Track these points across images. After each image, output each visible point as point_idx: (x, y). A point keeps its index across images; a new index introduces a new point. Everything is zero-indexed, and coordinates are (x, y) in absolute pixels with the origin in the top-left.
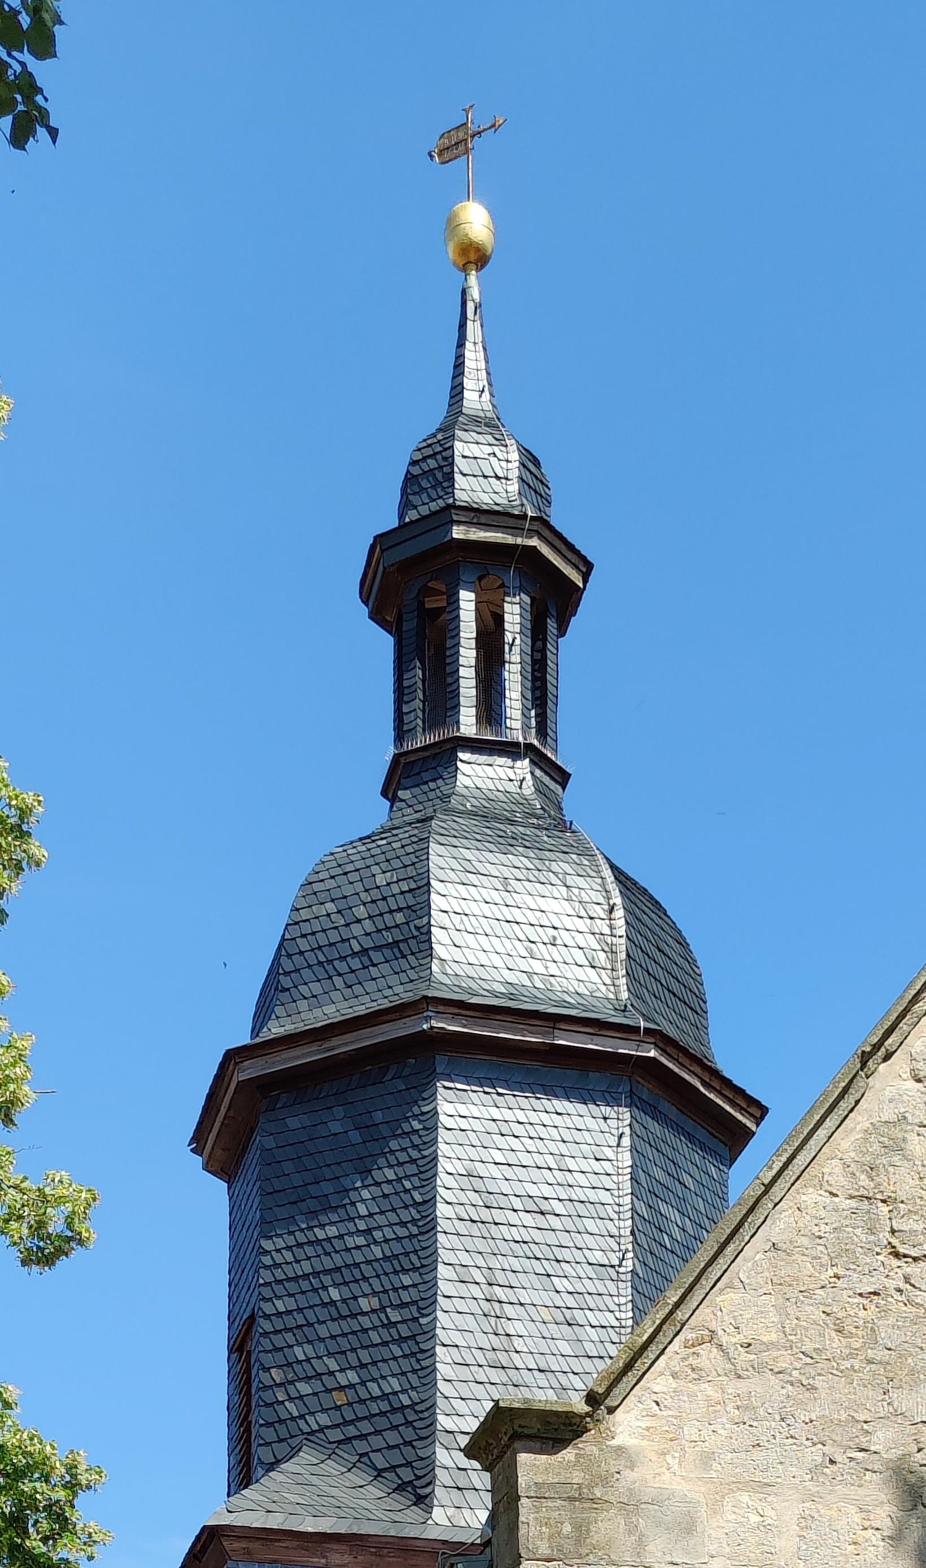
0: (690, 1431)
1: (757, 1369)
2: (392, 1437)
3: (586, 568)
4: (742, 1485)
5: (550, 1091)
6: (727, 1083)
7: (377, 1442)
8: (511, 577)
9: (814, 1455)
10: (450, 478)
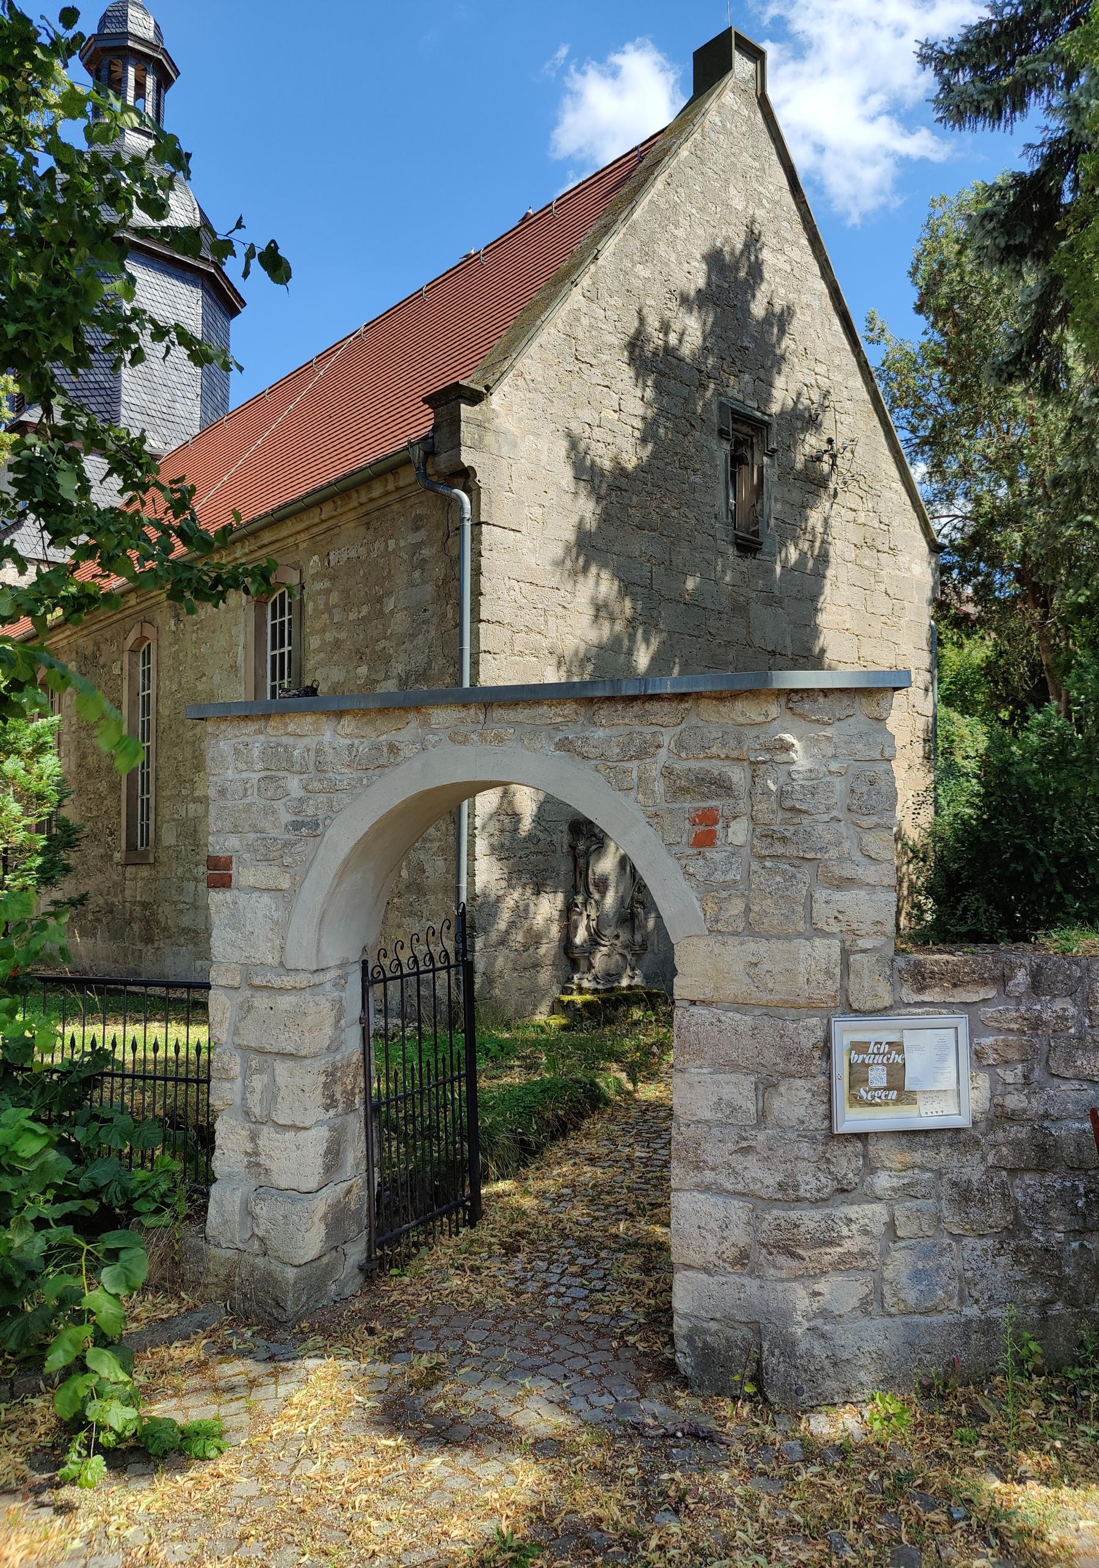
0: (515, 408)
1: (536, 390)
2: (100, 400)
3: (178, 74)
4: (529, 433)
5: (170, 275)
6: (235, 290)
7: (93, 400)
8: (150, 68)
9: (553, 426)
10: (126, 21)
